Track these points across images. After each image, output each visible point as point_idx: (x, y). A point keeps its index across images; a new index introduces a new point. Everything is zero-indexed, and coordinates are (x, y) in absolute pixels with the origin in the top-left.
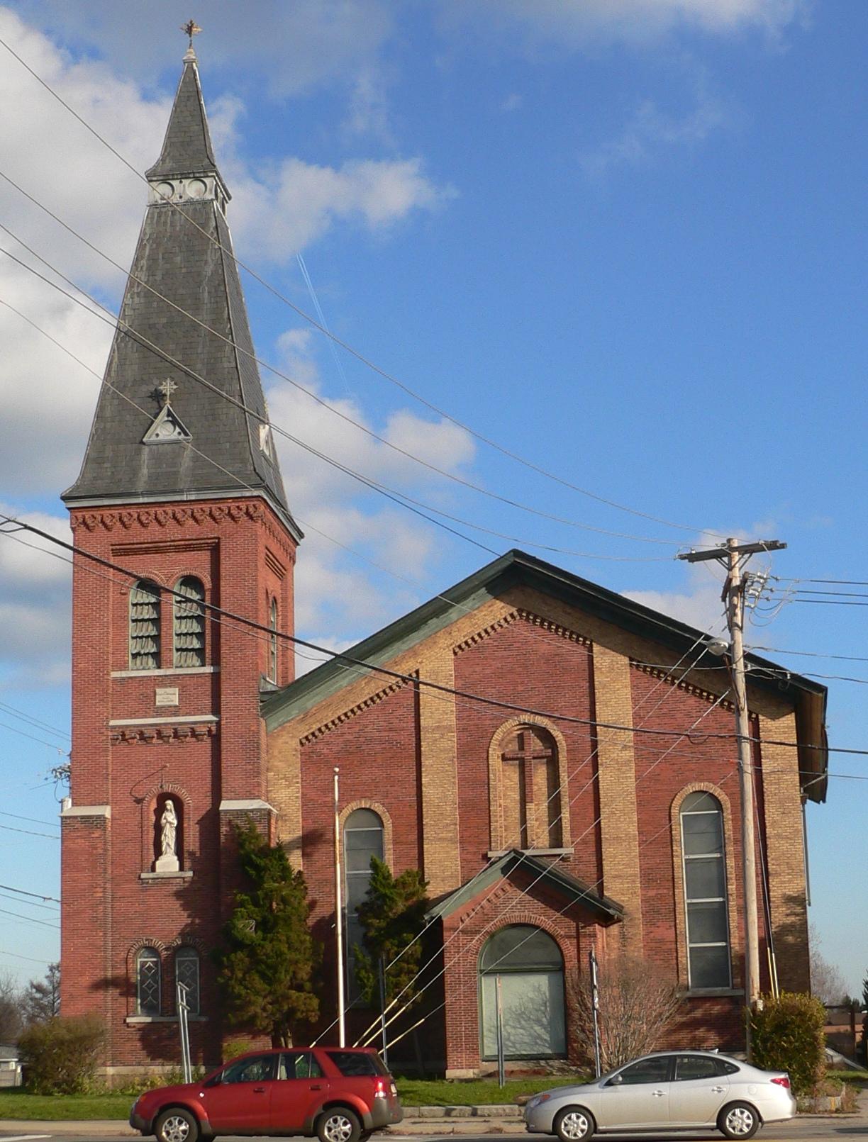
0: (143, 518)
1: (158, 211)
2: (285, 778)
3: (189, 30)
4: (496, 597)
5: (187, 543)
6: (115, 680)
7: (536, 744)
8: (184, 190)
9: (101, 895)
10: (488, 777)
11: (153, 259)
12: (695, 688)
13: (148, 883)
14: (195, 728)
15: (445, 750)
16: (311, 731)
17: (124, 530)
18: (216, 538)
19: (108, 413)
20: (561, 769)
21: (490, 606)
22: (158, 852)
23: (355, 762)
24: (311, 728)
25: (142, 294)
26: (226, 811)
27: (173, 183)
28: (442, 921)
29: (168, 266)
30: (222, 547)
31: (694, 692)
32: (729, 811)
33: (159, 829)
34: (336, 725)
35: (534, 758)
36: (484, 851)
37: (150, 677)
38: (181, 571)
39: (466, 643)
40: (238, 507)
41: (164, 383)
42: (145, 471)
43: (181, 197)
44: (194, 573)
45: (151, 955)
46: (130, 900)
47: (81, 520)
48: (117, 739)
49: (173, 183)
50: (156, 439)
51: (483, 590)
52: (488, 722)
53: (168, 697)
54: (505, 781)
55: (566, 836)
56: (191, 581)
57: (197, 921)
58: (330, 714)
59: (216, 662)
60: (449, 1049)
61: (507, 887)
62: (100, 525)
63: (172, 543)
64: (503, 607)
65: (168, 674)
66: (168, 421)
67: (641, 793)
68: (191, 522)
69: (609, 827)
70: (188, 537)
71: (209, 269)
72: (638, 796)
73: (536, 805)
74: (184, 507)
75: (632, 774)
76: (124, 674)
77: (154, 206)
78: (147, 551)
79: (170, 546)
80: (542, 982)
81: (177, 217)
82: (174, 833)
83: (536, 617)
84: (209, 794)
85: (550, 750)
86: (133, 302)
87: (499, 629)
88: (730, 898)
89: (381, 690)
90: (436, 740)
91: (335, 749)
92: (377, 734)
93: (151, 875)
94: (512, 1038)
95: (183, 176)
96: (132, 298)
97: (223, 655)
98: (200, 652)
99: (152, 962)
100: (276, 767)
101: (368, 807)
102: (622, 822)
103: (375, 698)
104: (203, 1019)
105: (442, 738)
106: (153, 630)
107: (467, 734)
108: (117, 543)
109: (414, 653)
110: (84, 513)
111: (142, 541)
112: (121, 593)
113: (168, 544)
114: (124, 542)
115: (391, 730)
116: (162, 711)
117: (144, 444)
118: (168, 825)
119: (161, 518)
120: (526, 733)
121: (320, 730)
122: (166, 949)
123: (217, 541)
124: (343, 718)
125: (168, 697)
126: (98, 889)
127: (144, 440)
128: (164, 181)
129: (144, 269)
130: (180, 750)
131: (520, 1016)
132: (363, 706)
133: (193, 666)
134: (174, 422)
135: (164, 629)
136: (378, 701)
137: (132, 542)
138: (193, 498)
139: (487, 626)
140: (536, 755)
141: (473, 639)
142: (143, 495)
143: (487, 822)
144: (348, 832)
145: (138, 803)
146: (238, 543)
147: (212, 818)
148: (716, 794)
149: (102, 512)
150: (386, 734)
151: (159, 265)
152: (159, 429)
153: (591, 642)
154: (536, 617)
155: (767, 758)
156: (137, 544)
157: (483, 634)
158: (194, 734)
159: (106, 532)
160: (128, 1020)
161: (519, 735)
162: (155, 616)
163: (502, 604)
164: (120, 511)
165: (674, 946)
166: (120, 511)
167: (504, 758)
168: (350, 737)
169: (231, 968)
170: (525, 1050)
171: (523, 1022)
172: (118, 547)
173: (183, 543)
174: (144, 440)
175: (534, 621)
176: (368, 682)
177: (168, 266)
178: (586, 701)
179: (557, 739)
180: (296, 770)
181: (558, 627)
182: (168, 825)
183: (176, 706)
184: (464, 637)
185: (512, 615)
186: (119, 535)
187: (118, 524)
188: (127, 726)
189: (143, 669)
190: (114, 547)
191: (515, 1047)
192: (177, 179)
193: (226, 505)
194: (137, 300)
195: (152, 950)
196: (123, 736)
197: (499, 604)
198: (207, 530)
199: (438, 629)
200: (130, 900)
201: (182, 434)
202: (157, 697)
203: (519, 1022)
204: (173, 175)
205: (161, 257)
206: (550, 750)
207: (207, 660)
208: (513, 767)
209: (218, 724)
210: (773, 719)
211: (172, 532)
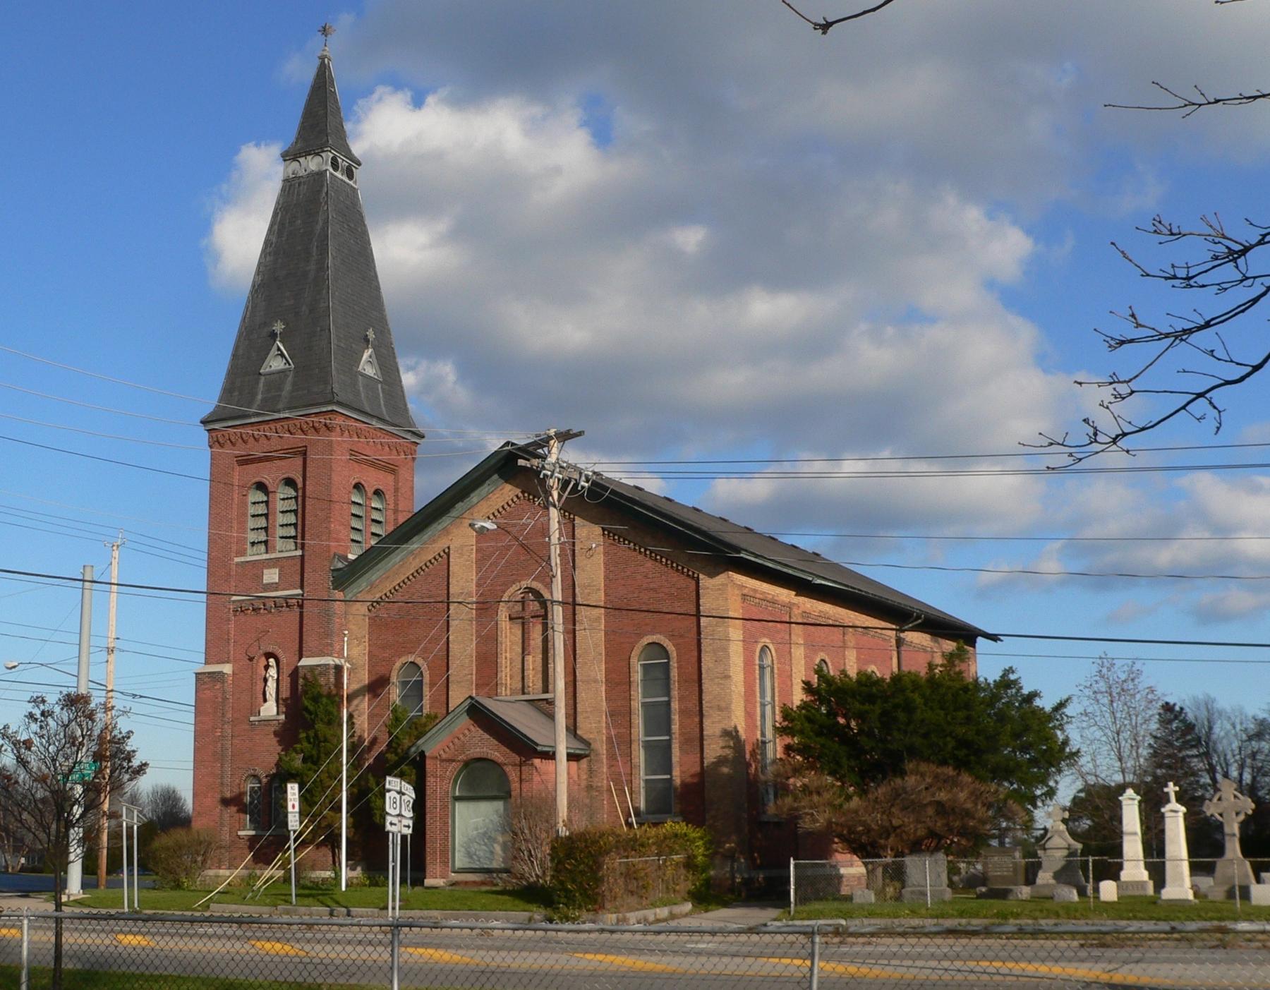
1: (289, 185)
2: (357, 639)
4: (507, 481)
6: (237, 564)
7: (534, 606)
11: (282, 224)
19: (241, 352)
32: (675, 660)
34: (392, 594)
35: (532, 617)
42: (259, 397)
46: (243, 738)
47: (215, 439)
49: (300, 160)
51: (496, 477)
54: (509, 636)
56: (290, 482)
60: (428, 862)
61: (472, 728)
71: (319, 227)
76: (242, 559)
77: (286, 181)
80: (499, 805)
81: (301, 188)
88: (674, 736)
102: (592, 671)
103: (420, 570)
109: (446, 531)
117: (260, 374)
124: (397, 588)
127: (262, 371)
130: (279, 618)
131: (487, 837)
132: (411, 577)
135: (270, 522)
136: (422, 573)
139: (499, 506)
144: (644, 666)
149: (243, 431)
170: (486, 864)
180: (365, 632)
185: (517, 496)
187: (240, 440)
191: (479, 861)
194: (268, 258)
197: (508, 487)
200: (243, 738)
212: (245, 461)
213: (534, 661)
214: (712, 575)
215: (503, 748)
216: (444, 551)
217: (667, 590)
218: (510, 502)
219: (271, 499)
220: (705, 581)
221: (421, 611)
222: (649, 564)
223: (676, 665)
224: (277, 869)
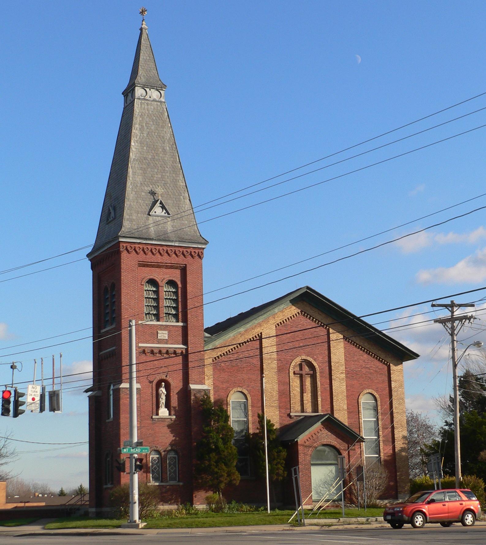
0: (154, 251)
3: (142, 12)
5: (172, 265)
7: (306, 369)
8: (152, 94)
10: (289, 381)
12: (367, 350)
16: (217, 355)
17: (145, 255)
18: (184, 264)
20: (317, 380)
21: (290, 308)
22: (158, 407)
26: (194, 390)
27: (148, 90)
28: (298, 442)
29: (148, 130)
30: (188, 269)
31: (366, 352)
32: (379, 402)
35: (306, 374)
36: (288, 413)
37: (155, 325)
38: (168, 278)
39: (281, 323)
40: (195, 252)
43: (150, 97)
44: (174, 279)
45: (156, 454)
50: (155, 214)
52: (289, 357)
53: (163, 335)
54: (295, 382)
55: (320, 408)
56: (171, 283)
57: (177, 439)
59: (185, 320)
61: (322, 429)
62: (134, 251)
63: (165, 264)
64: (295, 310)
65: (163, 324)
66: (160, 206)
68: (174, 255)
70: (173, 262)
74: (172, 248)
78: (153, 266)
80: (333, 468)
82: (165, 398)
83: (308, 315)
84: (181, 381)
85: (312, 371)
87: (293, 318)
93: (157, 417)
94: (322, 492)
95: (152, 87)
97: (189, 319)
98: (176, 316)
99: (156, 457)
101: (241, 390)
102: (341, 404)
104: (181, 484)
106: (154, 303)
108: (141, 261)
109: (260, 325)
111: (153, 261)
112: (141, 284)
113: (164, 264)
114: (144, 261)
116: (160, 341)
118: (163, 394)
119: (161, 252)
121: (221, 355)
122: (164, 451)
125: (163, 335)
129: (138, 129)
133: (173, 322)
137: (148, 261)
138: (177, 245)
140: (307, 373)
145: (150, 383)
146: (194, 268)
147: (185, 392)
148: (375, 395)
152: (156, 209)
153: (329, 327)
154: (308, 315)
155: (393, 381)
156: (150, 262)
158: (175, 353)
159: (136, 255)
161: (299, 364)
162: (155, 297)
163: (295, 308)
165: (360, 456)
166: (143, 246)
167: (294, 373)
169: (209, 460)
171: (326, 486)
173: (170, 264)
174: (150, 213)
175: (307, 316)
176: (241, 336)
177: (148, 130)
178: (327, 352)
179: (316, 367)
181: (316, 320)
182: (163, 394)
183: (166, 340)
184: (280, 320)
185: (298, 313)
186: (142, 257)
188: (146, 347)
189: (151, 321)
190: (139, 262)
192: (149, 88)
194: (137, 144)
195: (158, 452)
197: (294, 308)
198: (181, 260)
199: (270, 315)
201: (166, 214)
202: (159, 334)
203: (325, 486)
204: (147, 86)
206: (312, 371)
207: (180, 320)
208: (297, 378)
209: (187, 350)
210: (396, 366)
211: (166, 259)
213: (308, 396)
214: (396, 365)
215: (339, 440)
216: (258, 335)
217: (374, 369)
218: (295, 315)
220: (393, 367)
222: (366, 356)
223: (380, 404)
224: (321, 500)
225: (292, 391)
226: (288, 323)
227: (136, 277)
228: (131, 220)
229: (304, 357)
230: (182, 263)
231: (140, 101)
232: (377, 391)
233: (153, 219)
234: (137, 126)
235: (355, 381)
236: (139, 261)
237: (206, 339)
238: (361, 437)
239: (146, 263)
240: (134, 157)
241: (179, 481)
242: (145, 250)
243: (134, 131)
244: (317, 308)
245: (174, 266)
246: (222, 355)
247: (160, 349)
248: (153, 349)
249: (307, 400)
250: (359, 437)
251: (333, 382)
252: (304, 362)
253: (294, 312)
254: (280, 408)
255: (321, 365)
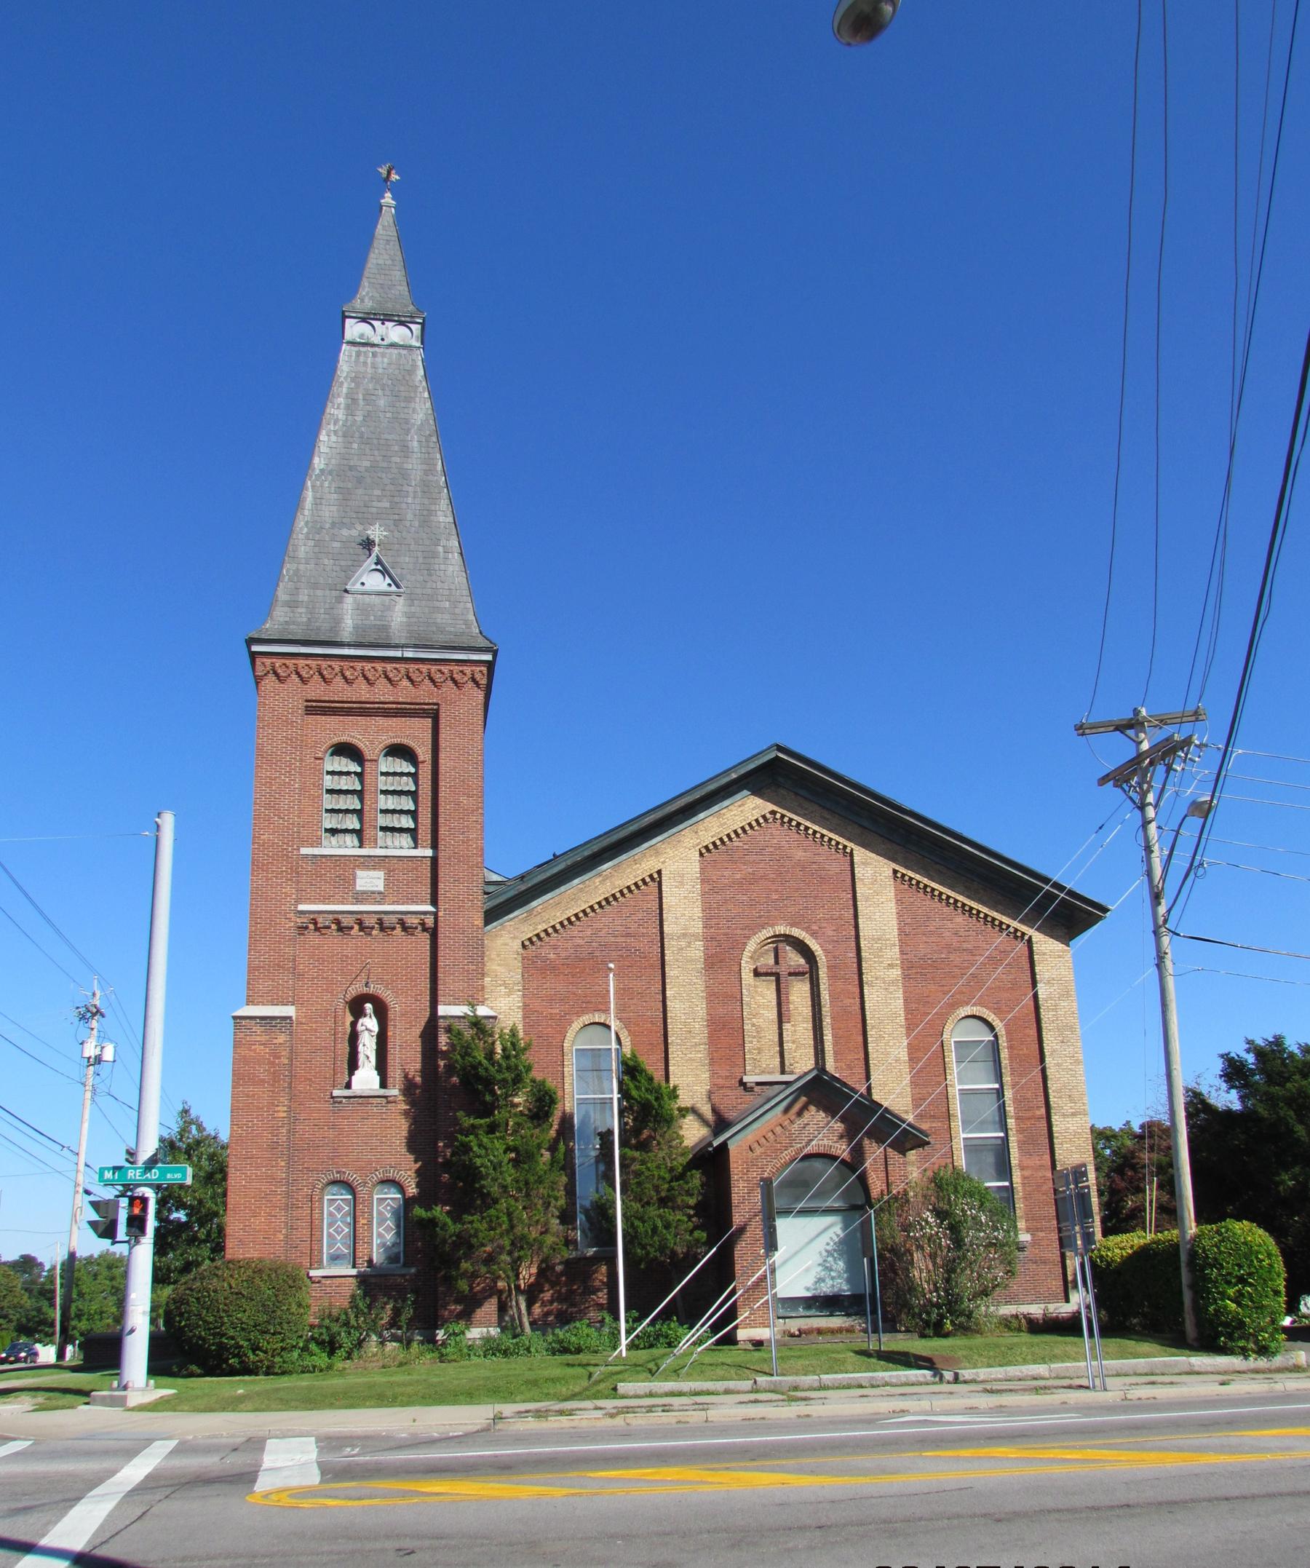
0: (348, 673)
2: (505, 985)
5: (399, 706)
7: (795, 960)
9: (285, 1115)
13: (341, 1102)
14: (405, 920)
15: (692, 960)
21: (740, 806)
22: (353, 1065)
23: (587, 970)
24: (536, 929)
25: (340, 433)
29: (370, 408)
33: (354, 1038)
35: (790, 974)
39: (714, 843)
40: (462, 672)
41: (382, 529)
43: (383, 340)
44: (405, 741)
48: (307, 928)
52: (739, 932)
54: (760, 998)
58: (558, 914)
67: (910, 1016)
68: (406, 683)
69: (877, 1051)
70: (401, 700)
72: (906, 1019)
73: (792, 1025)
74: (398, 666)
75: (900, 994)
76: (316, 851)
78: (349, 712)
79: (379, 708)
82: (374, 1040)
86: (329, 440)
89: (618, 890)
90: (682, 949)
91: (563, 955)
92: (613, 939)
96: (328, 436)
98: (413, 832)
100: (495, 971)
105: (689, 947)
107: (715, 943)
110: (274, 660)
111: (345, 699)
114: (323, 699)
115: (628, 935)
116: (362, 897)
120: (781, 945)
123: (435, 707)
126: (279, 1108)
128: (364, 320)
129: (342, 406)
134: (385, 572)
139: (737, 826)
140: (792, 971)
141: (721, 839)
142: (349, 645)
143: (741, 1042)
150: (623, 939)
151: (358, 405)
157: (733, 835)
160: (312, 1273)
164: (319, 662)
167: (757, 973)
168: (581, 942)
172: (314, 704)
173: (394, 706)
176: (604, 880)
177: (370, 408)
183: (380, 893)
186: (316, 690)
190: (309, 704)
193: (447, 667)
194: (334, 438)
196: (314, 924)
197: (758, 801)
198: (425, 694)
205: (361, 397)
209: (436, 915)
211: (383, 692)
212: (316, 709)
218: (754, 824)
219: (368, 770)
221: (614, 953)
225: (749, 1019)
226: (735, 844)
227: (297, 738)
228: (292, 605)
229: (781, 929)
230: (426, 701)
231: (355, 349)
232: (998, 1011)
233: (355, 600)
234: (341, 400)
235: (933, 987)
236: (307, 701)
237: (491, 889)
238: (908, 1125)
239: (327, 705)
240: (322, 466)
241: (405, 1265)
242: (325, 673)
243: (330, 410)
244: (815, 803)
245: (406, 709)
246: (550, 930)
247: (359, 917)
248: (340, 917)
249: (794, 1042)
250: (904, 1126)
251: (866, 991)
252: (781, 941)
253: (753, 815)
254: (712, 1062)
255: (831, 947)
